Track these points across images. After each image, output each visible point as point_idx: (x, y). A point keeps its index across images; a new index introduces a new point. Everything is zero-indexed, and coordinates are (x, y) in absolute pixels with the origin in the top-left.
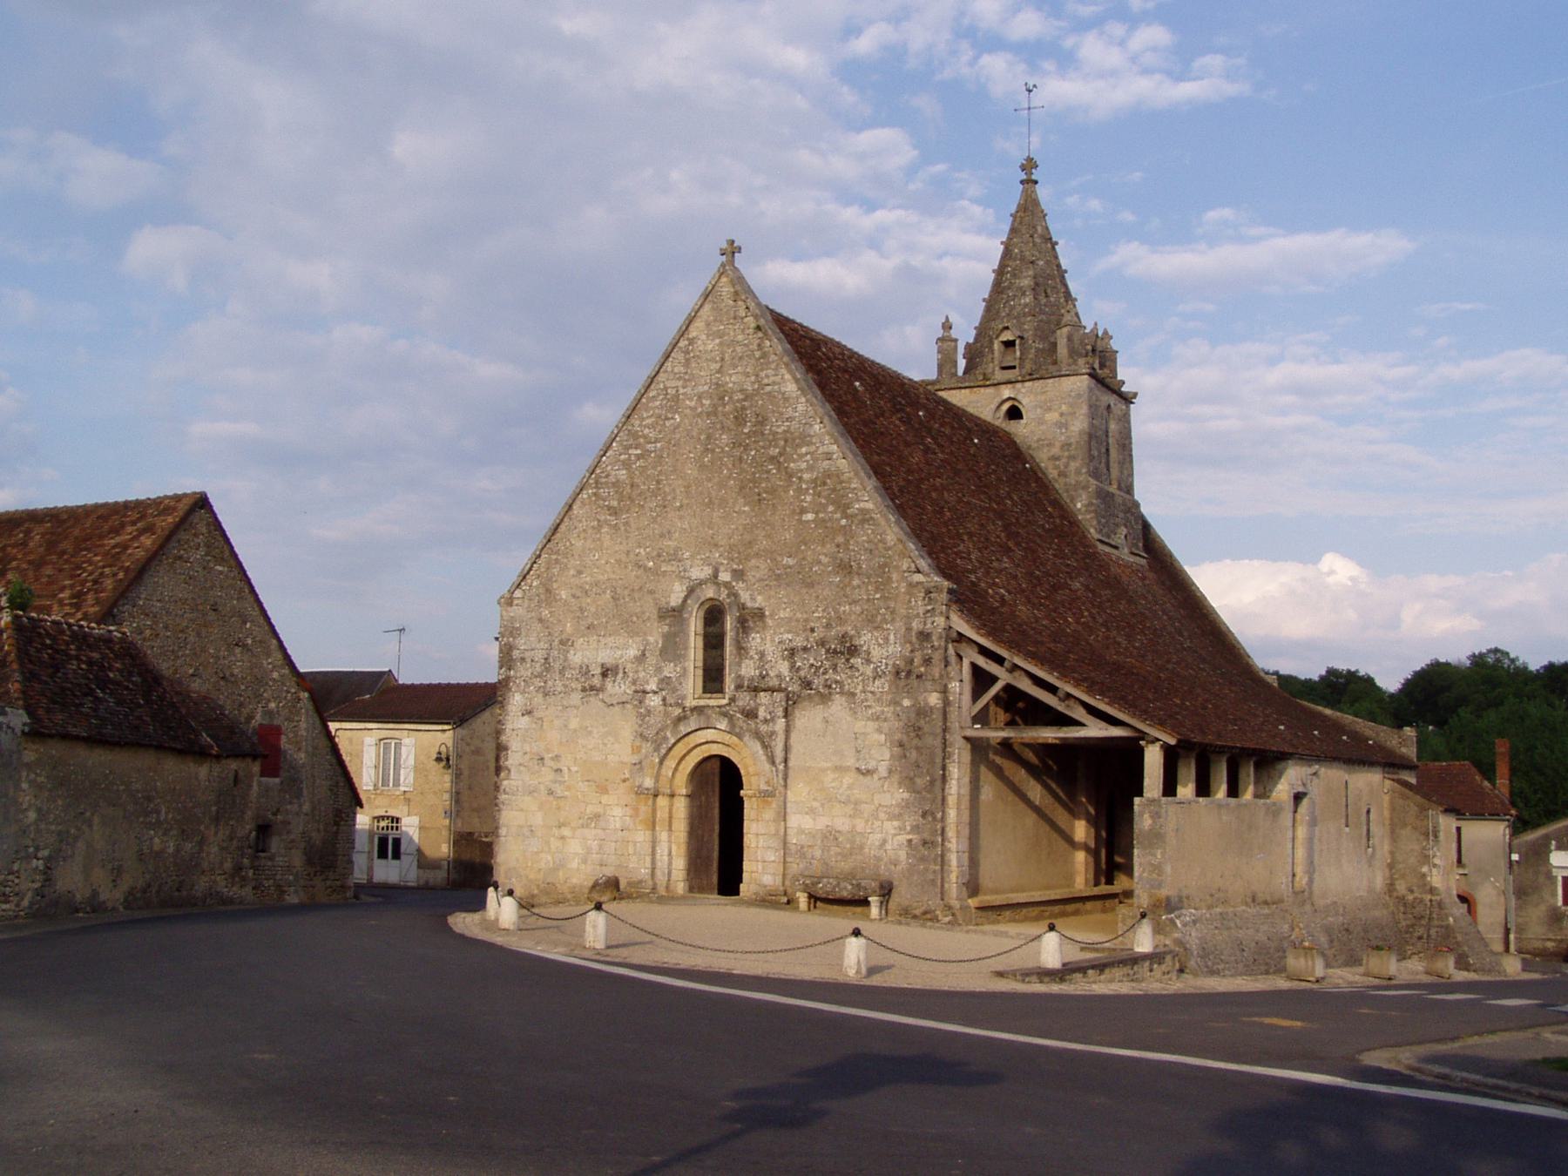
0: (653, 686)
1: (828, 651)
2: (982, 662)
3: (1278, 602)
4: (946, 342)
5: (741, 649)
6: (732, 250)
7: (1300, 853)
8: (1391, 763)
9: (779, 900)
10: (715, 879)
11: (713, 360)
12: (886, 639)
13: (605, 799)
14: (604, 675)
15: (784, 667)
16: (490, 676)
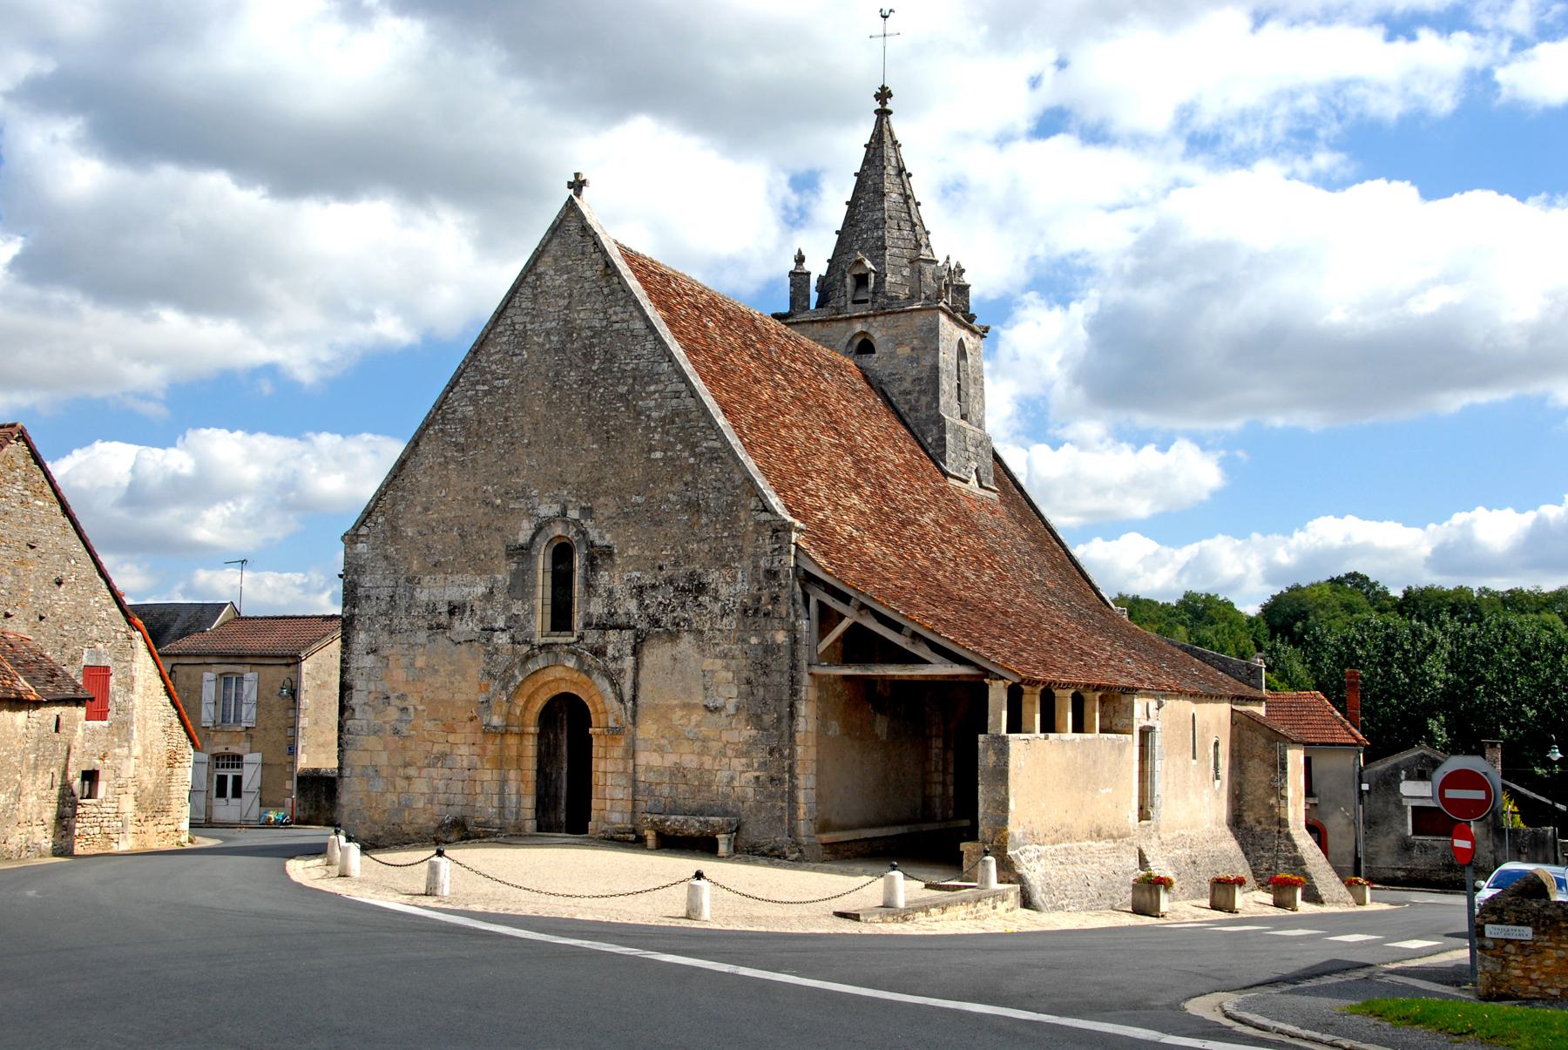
1: (676, 589)
2: (828, 600)
5: (589, 586)
9: (629, 840)
10: (563, 817)
12: (734, 577)
13: (451, 738)
14: (451, 613)
15: (632, 605)
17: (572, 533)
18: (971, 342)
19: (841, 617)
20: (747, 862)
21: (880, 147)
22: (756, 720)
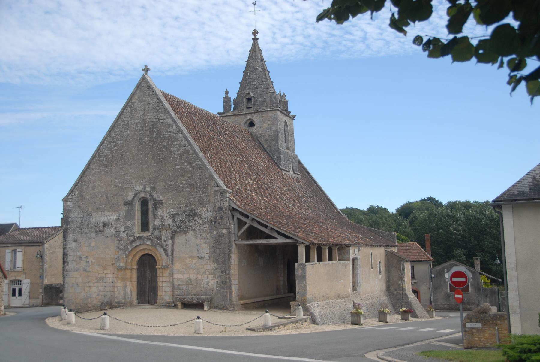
1: (186, 215)
2: (241, 217)
4: (227, 100)
5: (155, 215)
12: (207, 210)
13: (105, 271)
14: (104, 226)
15: (171, 221)
17: (148, 196)
19: (246, 223)
21: (255, 39)
22: (216, 261)
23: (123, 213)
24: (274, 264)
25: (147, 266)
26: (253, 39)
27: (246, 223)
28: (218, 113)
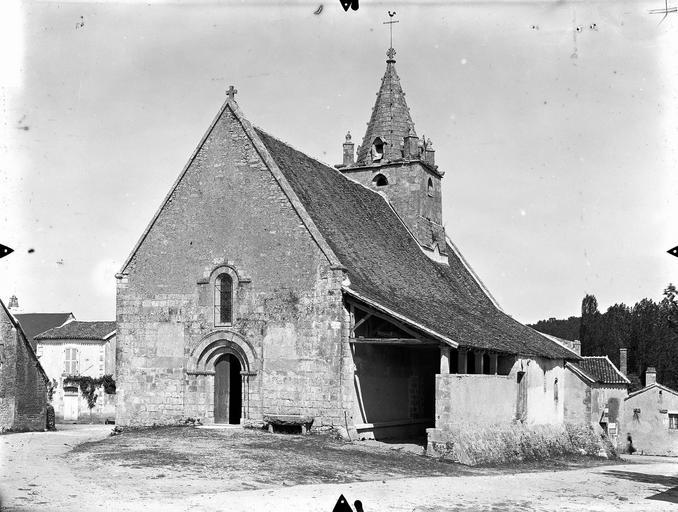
0: (195, 317)
2: (357, 306)
3: (527, 290)
4: (348, 146)
6: (232, 92)
7: (329, 251)
8: (567, 359)
11: (311, 310)
15: (261, 310)
16: (110, 316)
18: (433, 178)
19: (366, 314)
20: (427, 475)
21: (389, 76)
23: (195, 296)
24: (405, 369)
25: (232, 370)
26: (388, 62)
27: (366, 314)
28: (336, 167)
